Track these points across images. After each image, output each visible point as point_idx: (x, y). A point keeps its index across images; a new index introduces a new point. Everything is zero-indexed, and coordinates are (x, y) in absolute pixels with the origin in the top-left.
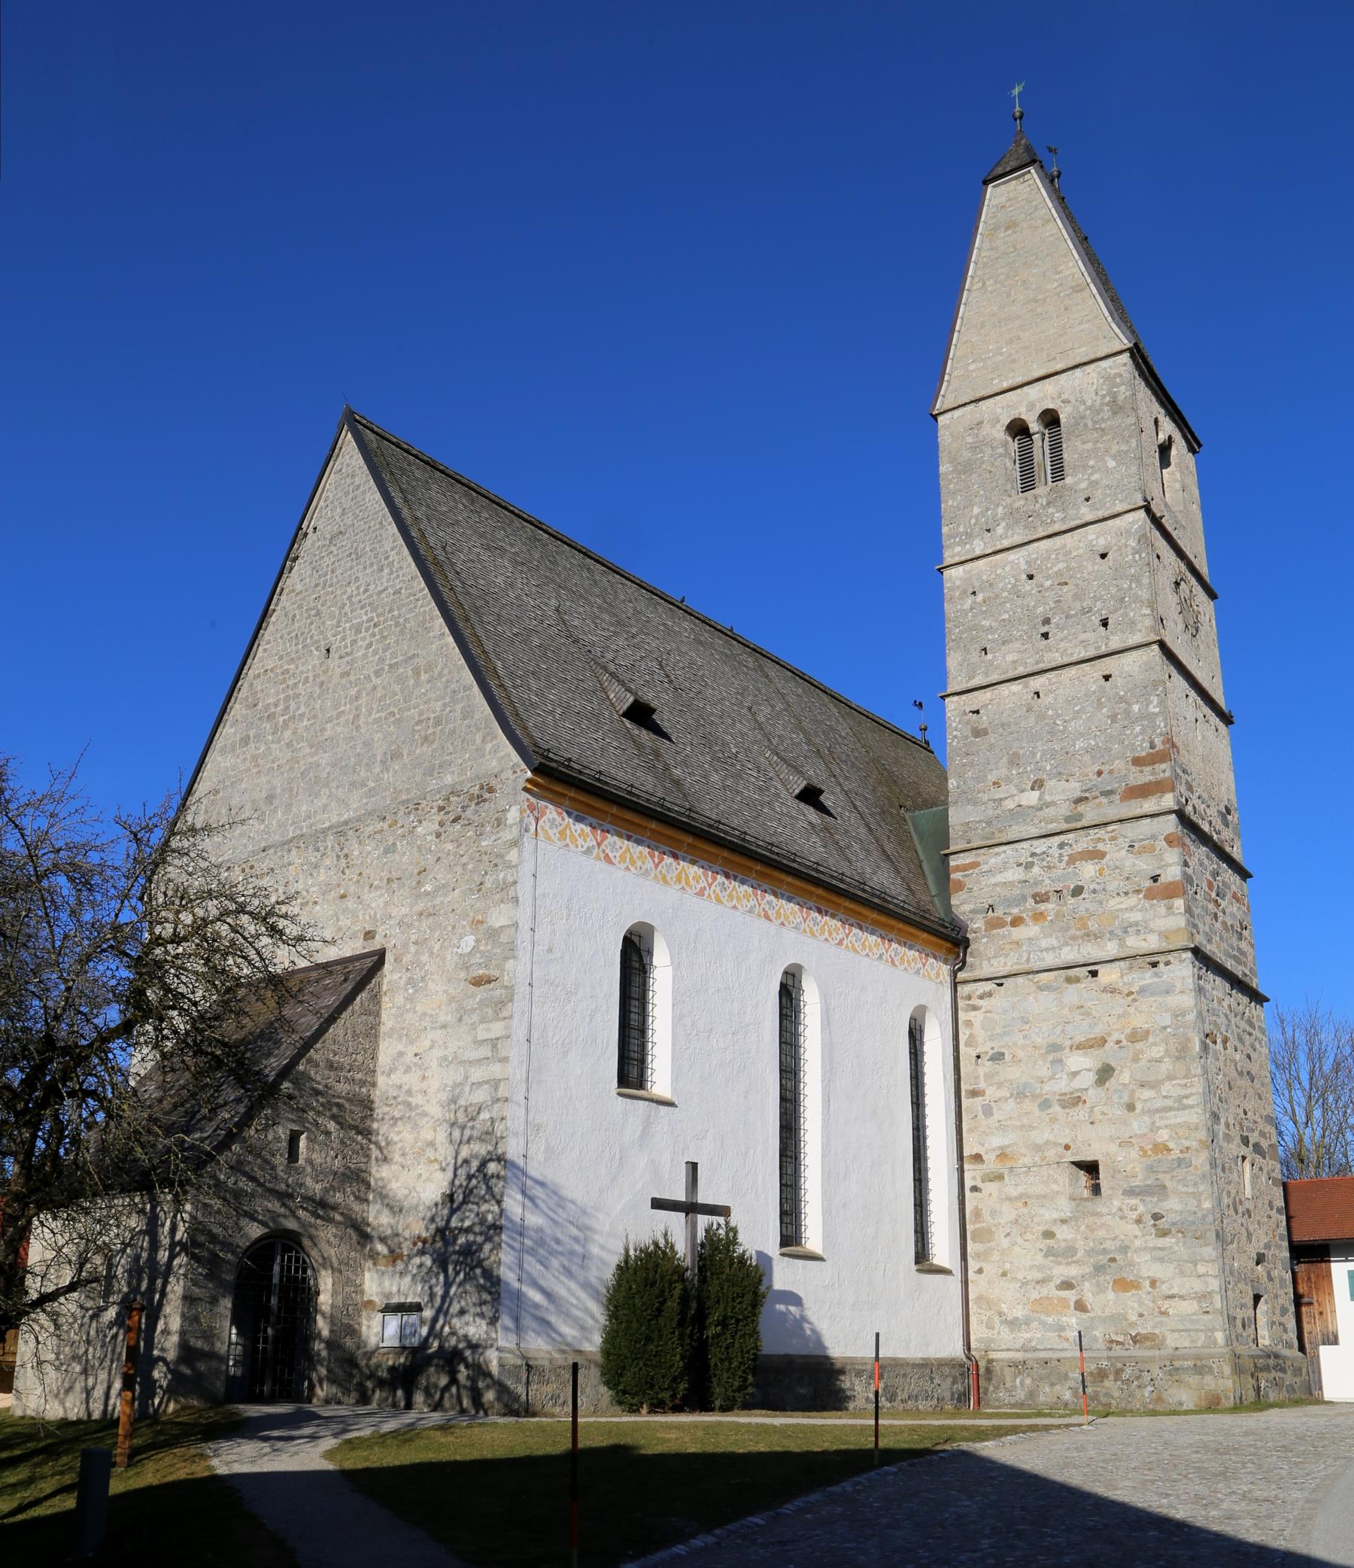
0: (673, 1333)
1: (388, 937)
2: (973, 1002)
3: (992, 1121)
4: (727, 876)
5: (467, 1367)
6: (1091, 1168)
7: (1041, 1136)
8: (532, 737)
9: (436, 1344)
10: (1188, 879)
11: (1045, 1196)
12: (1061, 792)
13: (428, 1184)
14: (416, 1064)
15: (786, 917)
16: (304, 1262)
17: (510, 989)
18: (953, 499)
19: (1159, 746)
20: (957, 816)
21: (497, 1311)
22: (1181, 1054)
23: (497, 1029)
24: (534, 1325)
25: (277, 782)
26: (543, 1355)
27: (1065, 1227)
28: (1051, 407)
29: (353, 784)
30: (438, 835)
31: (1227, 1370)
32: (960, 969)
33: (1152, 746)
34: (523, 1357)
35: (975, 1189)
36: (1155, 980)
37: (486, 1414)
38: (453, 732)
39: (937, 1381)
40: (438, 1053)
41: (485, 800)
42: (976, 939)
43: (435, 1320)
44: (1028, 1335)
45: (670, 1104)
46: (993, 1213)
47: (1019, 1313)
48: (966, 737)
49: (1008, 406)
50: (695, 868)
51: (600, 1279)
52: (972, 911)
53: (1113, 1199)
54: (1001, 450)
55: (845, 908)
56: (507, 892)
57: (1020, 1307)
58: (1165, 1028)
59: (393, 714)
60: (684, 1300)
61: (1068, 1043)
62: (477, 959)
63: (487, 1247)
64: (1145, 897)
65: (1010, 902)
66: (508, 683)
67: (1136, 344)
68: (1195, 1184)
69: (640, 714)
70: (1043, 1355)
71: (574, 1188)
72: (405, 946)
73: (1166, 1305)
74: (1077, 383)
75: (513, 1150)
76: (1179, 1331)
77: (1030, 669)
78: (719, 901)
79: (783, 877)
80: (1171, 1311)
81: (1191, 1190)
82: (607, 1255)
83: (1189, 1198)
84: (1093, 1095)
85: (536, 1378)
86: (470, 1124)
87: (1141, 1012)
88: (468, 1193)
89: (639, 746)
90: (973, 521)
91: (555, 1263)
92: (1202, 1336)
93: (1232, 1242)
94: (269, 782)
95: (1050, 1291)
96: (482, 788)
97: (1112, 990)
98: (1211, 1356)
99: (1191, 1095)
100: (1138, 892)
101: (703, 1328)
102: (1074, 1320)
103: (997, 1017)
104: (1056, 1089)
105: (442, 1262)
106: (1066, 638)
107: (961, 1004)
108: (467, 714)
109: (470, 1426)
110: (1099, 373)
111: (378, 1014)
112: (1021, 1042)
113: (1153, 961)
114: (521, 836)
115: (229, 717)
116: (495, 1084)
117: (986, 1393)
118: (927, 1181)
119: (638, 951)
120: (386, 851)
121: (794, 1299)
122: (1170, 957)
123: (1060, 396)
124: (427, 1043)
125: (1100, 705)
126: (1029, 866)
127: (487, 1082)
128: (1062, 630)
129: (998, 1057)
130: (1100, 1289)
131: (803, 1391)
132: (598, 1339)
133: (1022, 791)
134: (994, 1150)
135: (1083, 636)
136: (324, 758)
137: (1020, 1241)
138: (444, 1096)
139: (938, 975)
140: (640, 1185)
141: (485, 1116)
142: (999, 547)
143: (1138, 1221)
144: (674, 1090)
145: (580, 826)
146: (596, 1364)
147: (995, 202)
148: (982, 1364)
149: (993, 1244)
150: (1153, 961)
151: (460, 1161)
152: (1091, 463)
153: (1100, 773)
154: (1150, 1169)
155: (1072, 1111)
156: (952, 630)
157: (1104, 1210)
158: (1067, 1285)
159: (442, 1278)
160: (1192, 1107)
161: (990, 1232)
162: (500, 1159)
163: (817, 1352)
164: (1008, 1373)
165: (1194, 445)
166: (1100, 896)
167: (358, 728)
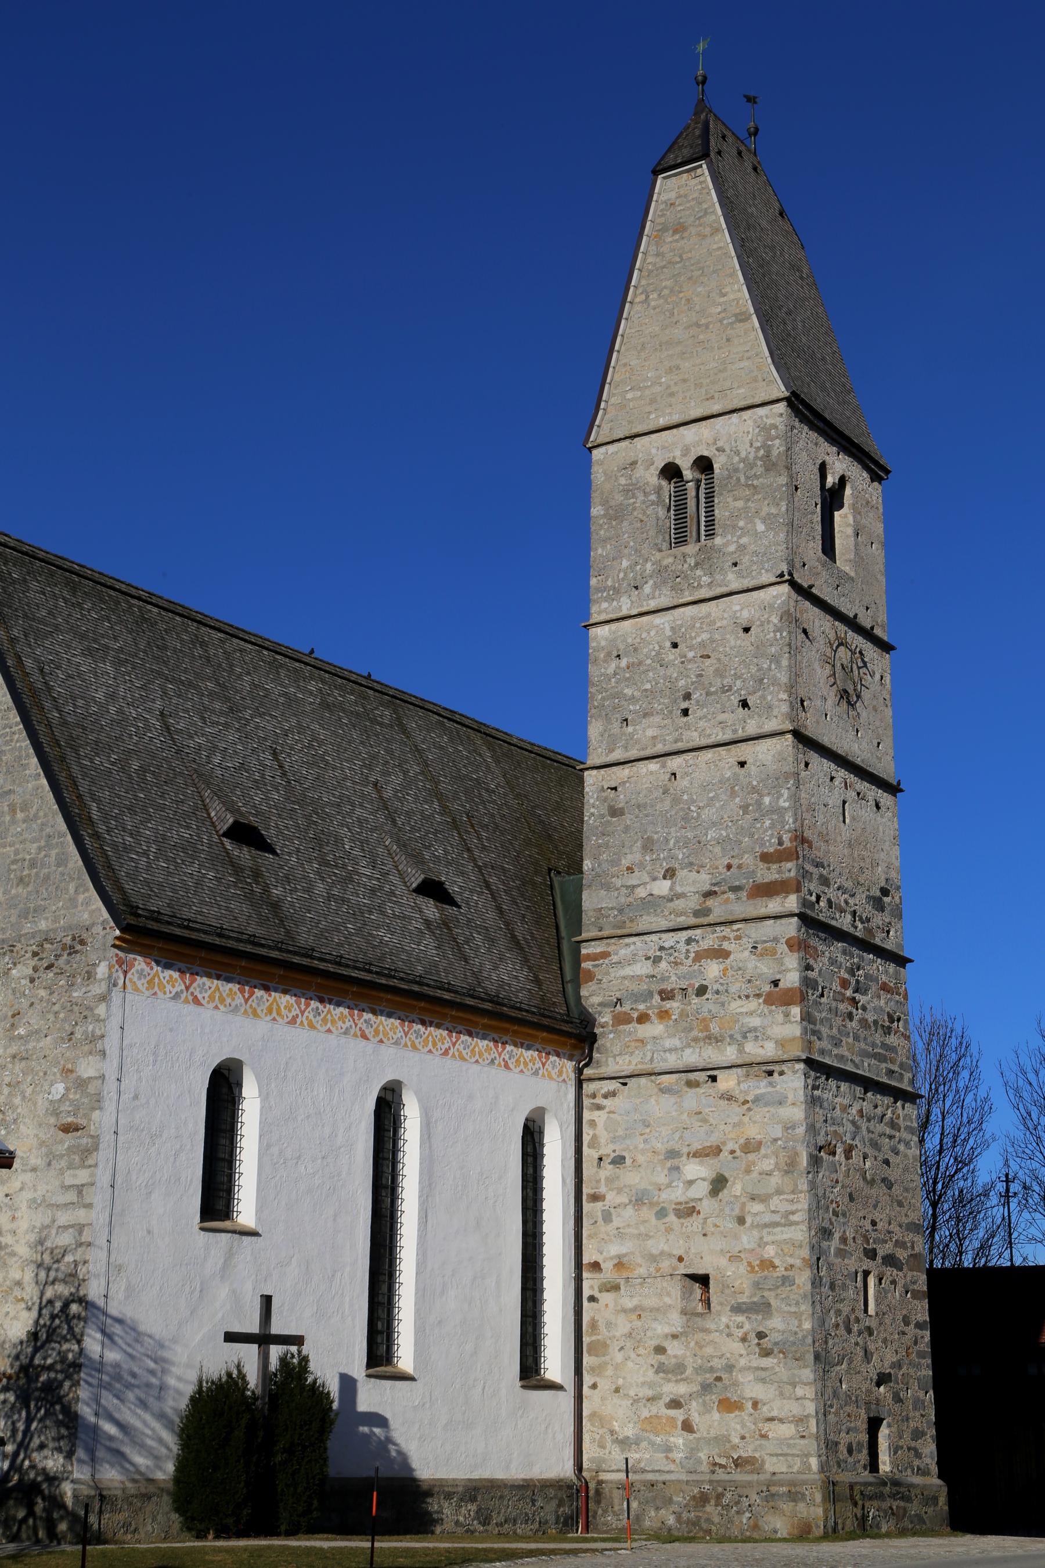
2: (599, 1100)
3: (611, 1228)
4: (322, 1001)
5: (44, 1499)
6: (703, 1280)
8: (121, 890)
9: (16, 1477)
10: (808, 983)
11: (658, 1310)
12: (693, 882)
13: (15, 1322)
14: (6, 1205)
15: (386, 1034)
17: (96, 1138)
18: (603, 548)
19: (787, 844)
20: (591, 900)
21: (74, 1445)
22: (789, 1169)
23: (82, 1176)
24: (108, 1456)
26: (117, 1485)
27: (675, 1342)
28: (706, 453)
30: (32, 980)
31: (818, 1497)
32: (587, 1065)
33: (780, 843)
34: (97, 1488)
35: (592, 1299)
36: (770, 1089)
37: (59, 1544)
38: (47, 878)
39: (539, 1504)
40: (27, 1195)
41: (76, 952)
42: (603, 1034)
43: (16, 1454)
44: (637, 1456)
45: (254, 1234)
46: (609, 1325)
47: (629, 1431)
48: (602, 816)
49: (664, 448)
50: (288, 997)
51: (175, 1409)
52: (600, 1004)
53: (723, 1318)
54: (653, 497)
55: (452, 1016)
56: (94, 1044)
57: (631, 1425)
58: (776, 1140)
61: (685, 1150)
62: (66, 1107)
63: (67, 1384)
64: (765, 1002)
65: (637, 997)
66: (102, 828)
67: (793, 393)
68: (797, 1304)
69: (244, 833)
70: (650, 1477)
71: (151, 1320)
73: (766, 1427)
74: (733, 429)
75: (94, 1291)
76: (777, 1455)
77: (668, 748)
78: (312, 1026)
80: (771, 1435)
81: (793, 1309)
82: (182, 1385)
83: (793, 1318)
84: (707, 1206)
85: (109, 1507)
86: (55, 1266)
87: (755, 1122)
88: (52, 1332)
89: (237, 869)
90: (621, 575)
91: (130, 1396)
92: (798, 1460)
93: (840, 1363)
96: (74, 939)
97: (729, 1097)
98: (804, 1482)
100: (758, 996)
102: (681, 1441)
103: (619, 1118)
104: (673, 1197)
105: (24, 1399)
106: (705, 717)
107: (586, 1102)
108: (62, 861)
109: (39, 1555)
110: (755, 421)
112: (641, 1146)
113: (768, 1069)
114: (110, 991)
116: (80, 1228)
117: (594, 1517)
118: (542, 1291)
119: (227, 1079)
121: (380, 1420)
122: (784, 1067)
123: (715, 443)
124: (18, 1185)
125: (733, 794)
126: (657, 960)
127: (72, 1226)
128: (702, 706)
130: (706, 1410)
132: (170, 1467)
133: (654, 879)
134: (611, 1258)
135: (722, 717)
137: (633, 1355)
138: (32, 1237)
139: (560, 1073)
140: (220, 1315)
141: (69, 1258)
142: (645, 609)
143: (744, 1340)
144: (258, 1219)
145: (168, 973)
146: (169, 1493)
148: (592, 1486)
149: (607, 1358)
150: (768, 1069)
151: (44, 1303)
152: (741, 524)
153: (729, 867)
154: (757, 1286)
155: (687, 1221)
156: (597, 697)
157: (713, 1327)
158: (675, 1404)
159: (24, 1414)
160: (797, 1223)
161: (605, 1345)
162: (81, 1300)
163: (403, 1474)
165: (877, 472)
166: (723, 998)
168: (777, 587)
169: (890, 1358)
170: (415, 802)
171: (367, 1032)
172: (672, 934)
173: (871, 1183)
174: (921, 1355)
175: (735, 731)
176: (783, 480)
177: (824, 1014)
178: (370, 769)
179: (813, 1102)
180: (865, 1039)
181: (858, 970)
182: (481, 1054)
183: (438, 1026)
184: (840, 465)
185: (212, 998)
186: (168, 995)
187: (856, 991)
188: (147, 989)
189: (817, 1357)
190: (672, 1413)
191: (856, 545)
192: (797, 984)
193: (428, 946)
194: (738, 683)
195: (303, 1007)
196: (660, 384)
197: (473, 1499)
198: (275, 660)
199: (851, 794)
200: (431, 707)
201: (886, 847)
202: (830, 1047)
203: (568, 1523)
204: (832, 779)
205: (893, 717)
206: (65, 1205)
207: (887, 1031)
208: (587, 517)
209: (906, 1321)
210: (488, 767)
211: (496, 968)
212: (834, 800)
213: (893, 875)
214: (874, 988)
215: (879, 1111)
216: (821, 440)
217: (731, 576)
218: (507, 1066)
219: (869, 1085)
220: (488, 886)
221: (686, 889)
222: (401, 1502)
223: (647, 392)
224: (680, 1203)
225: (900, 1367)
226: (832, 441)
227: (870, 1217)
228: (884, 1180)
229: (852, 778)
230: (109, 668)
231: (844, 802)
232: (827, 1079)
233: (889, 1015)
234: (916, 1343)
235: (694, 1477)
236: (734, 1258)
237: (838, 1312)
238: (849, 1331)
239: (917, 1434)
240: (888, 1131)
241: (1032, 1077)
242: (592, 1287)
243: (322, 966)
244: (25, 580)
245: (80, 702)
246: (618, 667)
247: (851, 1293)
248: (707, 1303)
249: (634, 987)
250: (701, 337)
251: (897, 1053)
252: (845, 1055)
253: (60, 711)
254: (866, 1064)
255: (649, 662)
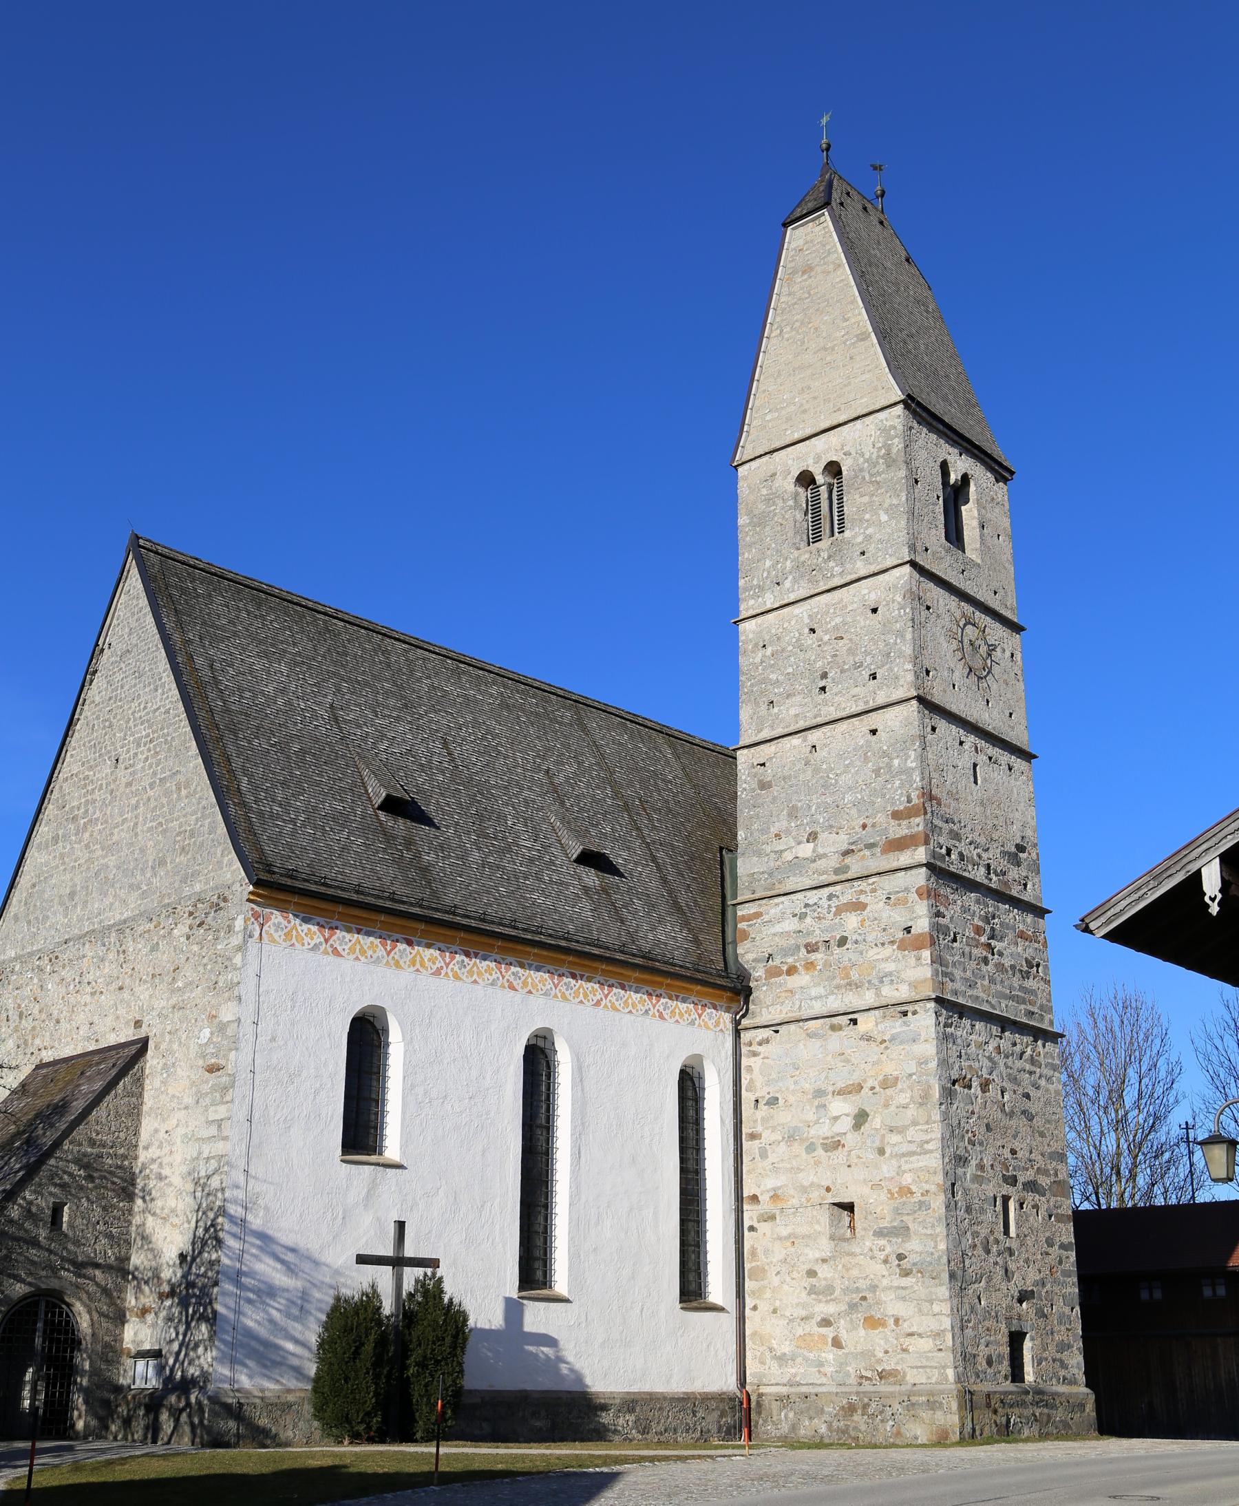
0: (368, 1373)
1: (151, 1028)
2: (755, 1048)
4: (467, 955)
6: (849, 1207)
7: (807, 1178)
12: (833, 843)
15: (534, 986)
16: (67, 1315)
18: (750, 552)
19: (915, 801)
22: (924, 1100)
23: (221, 1112)
25: (77, 880)
27: (825, 1266)
29: (131, 886)
31: (954, 1406)
32: (743, 1016)
35: (752, 1229)
36: (905, 1028)
38: (202, 844)
40: (181, 1131)
41: (220, 909)
44: (793, 1371)
46: (766, 1252)
47: (786, 1348)
48: (753, 790)
49: (798, 458)
53: (867, 1242)
54: (791, 503)
58: (911, 1075)
59: (161, 824)
60: (382, 1342)
61: (831, 1089)
62: (211, 1050)
65: (786, 952)
66: (250, 798)
67: (909, 396)
70: (804, 1389)
72: (162, 1034)
76: (917, 1367)
78: (457, 977)
79: (528, 949)
80: (911, 1349)
81: (929, 1232)
83: (930, 1240)
84: (851, 1139)
89: (389, 837)
94: (72, 879)
95: (812, 1327)
97: (868, 1038)
98: (942, 1392)
99: (931, 1140)
100: (892, 942)
101: (405, 1367)
102: (831, 1356)
103: (772, 1063)
107: (744, 1049)
110: (876, 425)
111: (141, 1095)
113: (903, 1009)
114: (245, 942)
115: (44, 817)
117: (756, 1426)
120: (152, 950)
121: (551, 1342)
124: (175, 1122)
126: (802, 916)
128: (838, 683)
129: (773, 1101)
131: (538, 1424)
135: (855, 691)
136: (112, 861)
137: (788, 1279)
138: (184, 1169)
139: (717, 1024)
140: (364, 1240)
142: (786, 601)
143: (886, 1261)
145: (305, 927)
147: (793, 245)
148: (753, 1398)
150: (903, 1009)
152: (867, 516)
153: (864, 826)
154: (897, 1211)
157: (858, 1250)
158: (825, 1322)
160: (931, 1151)
161: (764, 1270)
164: (775, 1406)
165: (1002, 473)
166: (861, 947)
167: (136, 834)
168: (899, 569)
169: (1032, 1276)
170: (587, 788)
171: (515, 983)
172: (815, 892)
173: (1011, 1115)
174: (1066, 1274)
175: (866, 703)
176: (903, 473)
177: (956, 958)
178: (544, 758)
179: (945, 1038)
180: (1002, 982)
181: (994, 918)
182: (634, 1005)
183: (589, 980)
184: (961, 465)
185: (352, 950)
186: (306, 946)
187: (992, 937)
188: (285, 940)
189: (952, 1276)
190: (823, 1330)
191: (982, 536)
192: (927, 930)
193: (585, 910)
194: (868, 659)
195: (448, 960)
196: (794, 404)
197: (631, 1410)
198: (458, 667)
199: (982, 759)
200: (613, 711)
201: (1021, 807)
202: (963, 988)
203: (731, 1433)
204: (961, 743)
205: (1025, 690)
206: (209, 1138)
207: (1026, 975)
208: (735, 527)
209: (1050, 1243)
210: (667, 762)
211: (653, 929)
212: (965, 761)
213: (1029, 833)
214: (1011, 935)
215: (1018, 1049)
216: (942, 442)
217: (859, 564)
218: (661, 1017)
219: (1005, 1024)
220: (654, 859)
221: (827, 850)
222: (571, 1412)
223: (783, 412)
224: (827, 1138)
225: (1044, 1285)
226: (954, 443)
227: (1009, 1147)
228: (1024, 1112)
229: (982, 744)
230: (283, 668)
231: (975, 765)
232: (961, 1018)
233: (1026, 960)
234: (1060, 1262)
235: (843, 1389)
236: (876, 1186)
237: (975, 1234)
238: (988, 1252)
239: (1063, 1347)
240: (1028, 1067)
241: (1218, 1042)
242: (751, 1218)
243: (465, 921)
244: (210, 595)
245: (247, 694)
246: (764, 656)
247: (989, 1216)
248: (852, 1227)
249: (783, 942)
250: (828, 358)
251: (1036, 996)
252: (981, 996)
253: (224, 701)
254: (1003, 1005)
255: (790, 648)
